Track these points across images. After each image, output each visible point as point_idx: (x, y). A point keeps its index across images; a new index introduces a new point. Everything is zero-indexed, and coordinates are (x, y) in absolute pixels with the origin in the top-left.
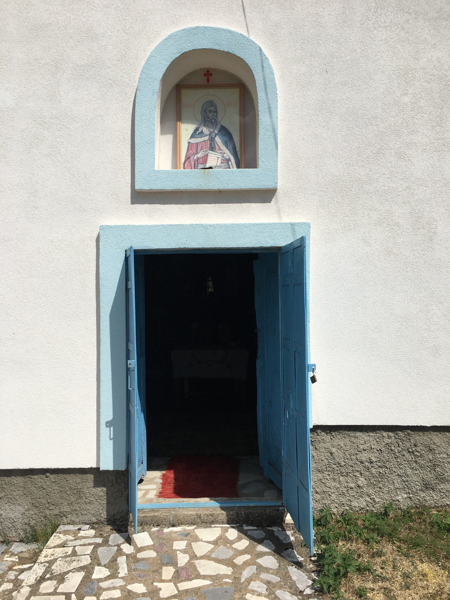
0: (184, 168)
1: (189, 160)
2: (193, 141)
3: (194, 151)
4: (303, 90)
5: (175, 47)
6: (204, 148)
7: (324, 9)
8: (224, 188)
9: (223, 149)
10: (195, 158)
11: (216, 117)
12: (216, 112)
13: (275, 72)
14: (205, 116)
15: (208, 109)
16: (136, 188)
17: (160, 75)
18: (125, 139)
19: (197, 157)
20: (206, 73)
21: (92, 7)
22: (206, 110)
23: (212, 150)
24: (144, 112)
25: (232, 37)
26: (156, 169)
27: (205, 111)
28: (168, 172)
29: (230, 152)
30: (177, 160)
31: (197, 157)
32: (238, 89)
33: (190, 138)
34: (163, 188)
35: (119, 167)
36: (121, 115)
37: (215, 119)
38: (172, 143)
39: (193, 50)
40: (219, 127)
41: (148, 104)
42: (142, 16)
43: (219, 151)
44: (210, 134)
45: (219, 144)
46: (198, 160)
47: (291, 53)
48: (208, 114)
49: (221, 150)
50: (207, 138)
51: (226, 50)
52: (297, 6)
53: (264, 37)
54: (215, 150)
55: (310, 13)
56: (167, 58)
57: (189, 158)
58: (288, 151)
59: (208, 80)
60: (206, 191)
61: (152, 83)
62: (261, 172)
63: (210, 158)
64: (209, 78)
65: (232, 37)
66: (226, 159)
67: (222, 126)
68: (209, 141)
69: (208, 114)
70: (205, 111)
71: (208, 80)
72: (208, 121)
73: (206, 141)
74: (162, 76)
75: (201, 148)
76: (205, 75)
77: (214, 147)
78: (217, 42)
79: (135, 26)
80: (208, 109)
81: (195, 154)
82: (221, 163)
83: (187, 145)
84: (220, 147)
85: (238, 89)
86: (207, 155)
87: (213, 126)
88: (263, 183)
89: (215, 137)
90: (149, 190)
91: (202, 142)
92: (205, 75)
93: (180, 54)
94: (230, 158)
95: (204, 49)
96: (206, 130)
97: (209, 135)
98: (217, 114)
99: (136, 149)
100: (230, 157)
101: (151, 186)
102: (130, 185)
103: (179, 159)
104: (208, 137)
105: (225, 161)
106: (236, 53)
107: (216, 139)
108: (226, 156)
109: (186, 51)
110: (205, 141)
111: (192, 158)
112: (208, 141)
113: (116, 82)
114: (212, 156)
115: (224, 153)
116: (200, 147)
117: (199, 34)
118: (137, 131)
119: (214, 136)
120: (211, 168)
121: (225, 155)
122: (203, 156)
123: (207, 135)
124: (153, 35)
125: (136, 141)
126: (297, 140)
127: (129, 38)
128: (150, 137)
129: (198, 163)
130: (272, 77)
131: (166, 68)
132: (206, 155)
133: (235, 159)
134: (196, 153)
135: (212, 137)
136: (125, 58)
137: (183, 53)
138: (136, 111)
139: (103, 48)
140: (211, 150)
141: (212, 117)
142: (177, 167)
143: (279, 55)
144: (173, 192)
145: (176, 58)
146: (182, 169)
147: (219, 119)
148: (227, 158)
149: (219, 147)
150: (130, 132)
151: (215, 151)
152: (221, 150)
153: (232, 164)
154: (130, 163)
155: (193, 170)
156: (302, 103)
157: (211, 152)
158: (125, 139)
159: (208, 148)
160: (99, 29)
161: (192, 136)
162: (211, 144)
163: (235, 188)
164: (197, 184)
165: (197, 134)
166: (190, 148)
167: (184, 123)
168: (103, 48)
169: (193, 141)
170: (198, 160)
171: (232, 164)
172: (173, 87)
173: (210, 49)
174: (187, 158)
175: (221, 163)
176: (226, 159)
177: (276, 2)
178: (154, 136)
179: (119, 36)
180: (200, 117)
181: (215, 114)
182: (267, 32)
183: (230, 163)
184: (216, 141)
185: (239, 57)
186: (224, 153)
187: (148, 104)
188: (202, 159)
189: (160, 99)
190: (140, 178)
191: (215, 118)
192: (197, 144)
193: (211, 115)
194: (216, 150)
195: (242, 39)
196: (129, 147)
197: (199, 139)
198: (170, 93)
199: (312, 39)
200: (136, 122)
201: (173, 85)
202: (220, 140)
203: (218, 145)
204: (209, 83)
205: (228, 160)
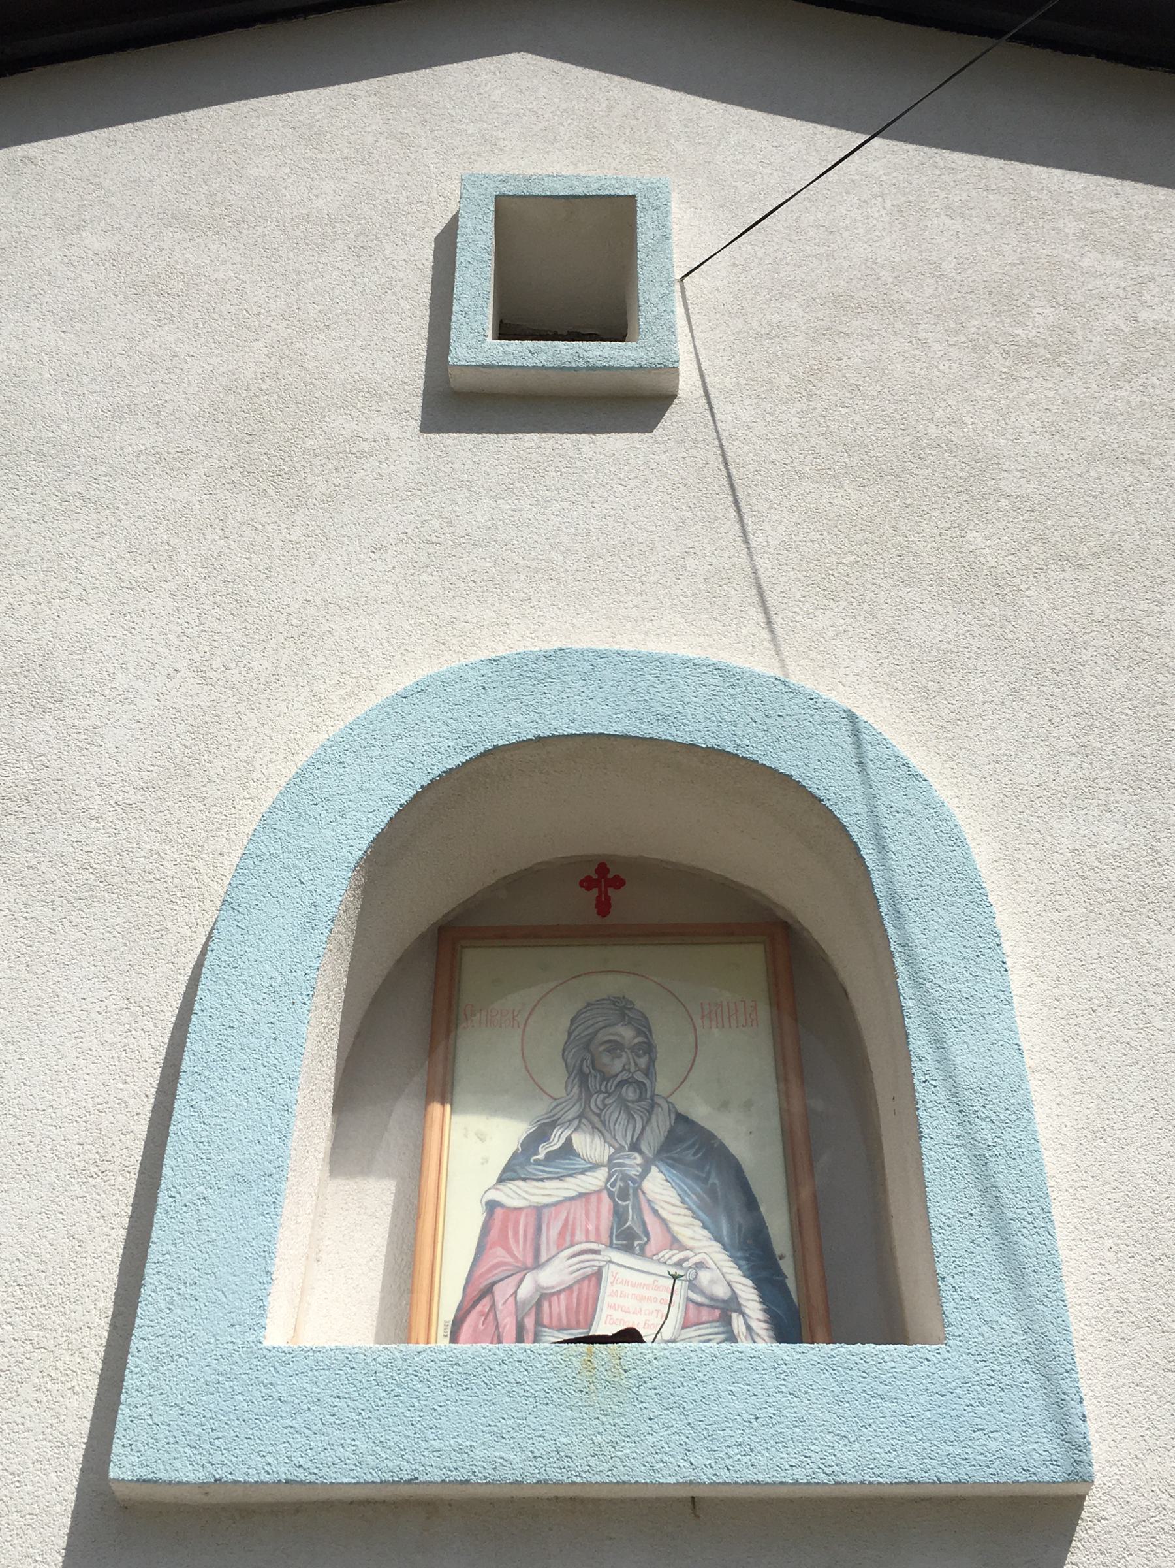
0: (454, 1338)
1: (486, 1302)
2: (516, 1195)
3: (521, 1250)
4: (1128, 925)
5: (444, 727)
6: (579, 1236)
7: (1160, 604)
8: (724, 1476)
9: (690, 1243)
10: (526, 1290)
11: (647, 1075)
12: (648, 1049)
13: (969, 832)
14: (586, 1070)
15: (602, 1036)
16: (114, 1472)
17: (361, 842)
18: (107, 1166)
19: (538, 1287)
20: (595, 877)
21: (63, 586)
22: (590, 1041)
23: (628, 1249)
24: (242, 1013)
25: (732, 691)
26: (267, 1343)
27: (587, 1047)
28: (347, 1359)
29: (735, 1259)
30: (410, 1304)
31: (538, 1287)
32: (761, 947)
33: (501, 1180)
34: (301, 1475)
35: (33, 1334)
36: (109, 1037)
37: (641, 1086)
38: (389, 1210)
39: (539, 739)
40: (660, 1126)
41: (274, 974)
42: (295, 622)
43: (666, 1254)
44: (610, 1159)
45: (664, 1214)
46: (539, 1305)
47: (1030, 767)
48: (606, 1059)
49: (685, 1248)
50: (595, 1180)
51: (704, 739)
52: (1027, 593)
53: (886, 703)
54: (642, 1248)
55: (1097, 616)
56: (399, 769)
57: (488, 1290)
58: (1109, 1242)
59: (603, 907)
60: (596, 1502)
61: (306, 877)
62: (967, 1372)
63: (613, 1307)
64: (608, 899)
65: (732, 691)
66: (714, 1303)
67: (682, 1119)
68: (611, 1195)
69: (606, 1059)
70: (587, 1047)
71: (603, 907)
72: (600, 1092)
73: (594, 1199)
74: (364, 846)
75: (562, 1234)
76: (587, 883)
77: (638, 1230)
78: (658, 707)
79: (258, 656)
80: (602, 1036)
81: (523, 1270)
82: (685, 1326)
83: (478, 1217)
84: (675, 1229)
85: (761, 947)
86: (598, 1275)
87: (631, 1117)
88: (993, 1445)
89: (643, 1176)
90: (202, 1485)
91: (567, 1204)
92: (587, 883)
93: (471, 755)
94: (734, 1297)
95: (593, 735)
96: (589, 1146)
97: (610, 1163)
98: (652, 1061)
99: (159, 1215)
100: (739, 1289)
101: (217, 1458)
102: (78, 1454)
103: (423, 1298)
104: (602, 1173)
105: (705, 1314)
106: (755, 754)
107: (647, 1185)
108: (712, 1282)
109: (500, 743)
110: (581, 1195)
111: (502, 1292)
112: (605, 1195)
113: (117, 879)
114: (625, 1282)
115: (700, 1265)
116: (554, 1232)
117: (568, 679)
118: (188, 1111)
119: (634, 1172)
120: (630, 1336)
121: (704, 1277)
122: (569, 1279)
123: (595, 1167)
124: (341, 692)
125: (166, 1171)
126: (1149, 1182)
127: (219, 700)
128: (258, 1148)
129: (538, 1323)
130: (958, 853)
131: (390, 811)
132: (589, 1277)
133: (764, 1298)
134: (529, 1262)
135: (625, 1177)
136: (188, 780)
137: (486, 753)
138: (197, 1007)
139: (82, 737)
140: (619, 1248)
141: (624, 1076)
142: (409, 1327)
143: (974, 772)
144: (367, 1502)
145: (450, 772)
146: (444, 1342)
147: (662, 1085)
148: (721, 1292)
149: (669, 1230)
150: (141, 1128)
151: (642, 1254)
152: (685, 1248)
153: (749, 1328)
154: (107, 1305)
155: (510, 1345)
156: (1136, 990)
157: (617, 1256)
158: (107, 1166)
159: (605, 1237)
160: (78, 663)
161: (511, 1172)
162: (619, 1215)
163: (801, 1475)
164: (543, 1446)
165: (538, 1162)
166: (494, 1233)
167: (465, 1111)
168: (82, 737)
169: (516, 1195)
170: (539, 1305)
171: (749, 1328)
172: (422, 937)
173: (626, 737)
174: (473, 1292)
175: (685, 1326)
176: (711, 1298)
177: (927, 578)
178: (284, 1138)
179: (174, 692)
180: (557, 1081)
181: (643, 1062)
182: (900, 685)
183: (737, 1323)
184: (650, 1196)
185: (774, 772)
186: (700, 1265)
187: (274, 974)
188: (569, 1298)
189: (346, 965)
190: (156, 1400)
191: (639, 1077)
192: (539, 1211)
193: (617, 1065)
194: (651, 1248)
195: (786, 696)
196: (121, 1208)
197: (547, 1184)
198: (403, 964)
199: (1128, 711)
200: (186, 1065)
201: (423, 928)
202: (673, 1193)
203: (664, 1221)
204: (609, 920)
205: (727, 1308)
